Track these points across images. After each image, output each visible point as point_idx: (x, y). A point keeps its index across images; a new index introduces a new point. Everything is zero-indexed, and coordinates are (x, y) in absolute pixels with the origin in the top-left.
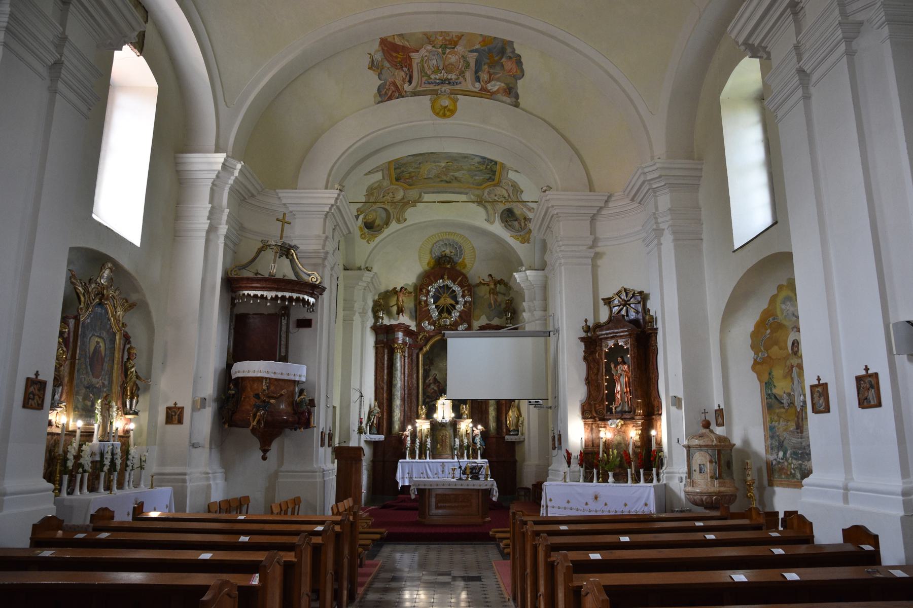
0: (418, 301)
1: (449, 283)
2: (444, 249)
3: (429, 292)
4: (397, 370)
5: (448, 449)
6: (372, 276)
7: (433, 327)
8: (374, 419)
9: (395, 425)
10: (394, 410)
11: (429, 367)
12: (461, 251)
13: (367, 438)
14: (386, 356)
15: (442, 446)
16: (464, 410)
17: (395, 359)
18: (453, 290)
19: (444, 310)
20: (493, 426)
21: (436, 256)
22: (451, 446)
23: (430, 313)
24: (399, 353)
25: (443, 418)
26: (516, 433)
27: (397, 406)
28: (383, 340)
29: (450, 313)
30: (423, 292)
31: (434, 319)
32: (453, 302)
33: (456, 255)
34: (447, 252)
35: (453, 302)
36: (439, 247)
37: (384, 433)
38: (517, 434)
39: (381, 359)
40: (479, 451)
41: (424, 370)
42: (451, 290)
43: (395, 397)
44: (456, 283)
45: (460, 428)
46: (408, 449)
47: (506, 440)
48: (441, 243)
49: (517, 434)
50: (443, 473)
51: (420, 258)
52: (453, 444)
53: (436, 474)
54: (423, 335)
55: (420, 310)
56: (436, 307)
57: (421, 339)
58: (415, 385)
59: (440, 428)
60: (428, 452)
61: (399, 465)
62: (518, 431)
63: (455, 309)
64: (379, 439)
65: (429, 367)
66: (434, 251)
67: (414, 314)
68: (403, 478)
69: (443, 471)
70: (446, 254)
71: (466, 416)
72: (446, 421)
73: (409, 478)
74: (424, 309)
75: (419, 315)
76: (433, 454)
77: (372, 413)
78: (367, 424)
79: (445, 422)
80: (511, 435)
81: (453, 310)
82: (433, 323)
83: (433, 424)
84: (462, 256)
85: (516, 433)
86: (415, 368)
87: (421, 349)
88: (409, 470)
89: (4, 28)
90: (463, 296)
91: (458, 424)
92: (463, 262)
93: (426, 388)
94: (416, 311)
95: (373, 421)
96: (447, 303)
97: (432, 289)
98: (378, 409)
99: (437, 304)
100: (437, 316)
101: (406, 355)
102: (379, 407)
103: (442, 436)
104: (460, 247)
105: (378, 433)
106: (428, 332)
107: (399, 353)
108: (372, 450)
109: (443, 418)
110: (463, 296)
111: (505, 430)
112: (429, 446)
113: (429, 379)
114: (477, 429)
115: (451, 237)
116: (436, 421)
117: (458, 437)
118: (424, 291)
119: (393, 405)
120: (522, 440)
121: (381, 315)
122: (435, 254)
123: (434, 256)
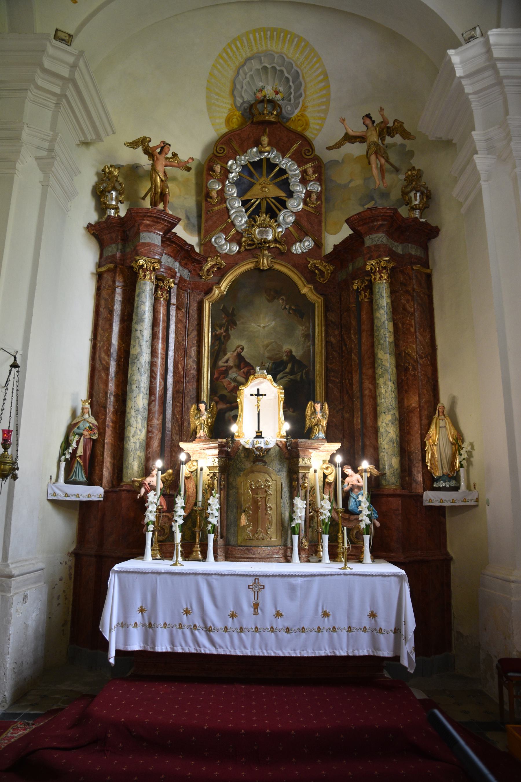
0: (204, 192)
1: (273, 155)
2: (261, 84)
3: (227, 172)
4: (142, 321)
5: (272, 530)
6: (71, 60)
7: (235, 248)
8: (78, 443)
9: (131, 459)
10: (128, 421)
11: (227, 331)
12: (298, 87)
13: (55, 494)
14: (119, 291)
15: (255, 520)
16: (319, 416)
17: (138, 295)
18: (281, 169)
19: (260, 209)
20: (391, 466)
21: (244, 102)
22: (282, 521)
23: (229, 217)
24: (148, 281)
25: (259, 435)
26: (453, 483)
27: (137, 411)
28: (114, 256)
29: (274, 216)
30: (214, 171)
31: (240, 230)
32: (281, 194)
33: (287, 98)
34: (269, 92)
35: (281, 194)
36: (251, 76)
37: (105, 481)
38: (456, 489)
39: (106, 300)
40: (367, 538)
41: (215, 338)
42: (277, 169)
43: (134, 387)
44: (288, 155)
45: (308, 468)
46: (151, 527)
47: (426, 503)
48: (255, 65)
49: (456, 489)
50: (256, 613)
51: (209, 107)
52: (287, 514)
53: (233, 615)
54: (213, 263)
55: (207, 212)
56: (244, 203)
57: (208, 270)
58: (194, 372)
59: (248, 465)
60: (211, 537)
61: (114, 582)
62: (457, 478)
63: (285, 208)
64: (89, 496)
65: (227, 331)
66: (238, 86)
67: (194, 221)
68: (124, 625)
69: (256, 606)
70: (265, 96)
71: (322, 435)
72: (267, 443)
73: (144, 625)
74: (216, 208)
75: (206, 221)
76: (227, 544)
77: (75, 430)
78: (60, 457)
79: (262, 445)
80: (439, 489)
81: (280, 210)
82: (237, 239)
83: (228, 453)
84: (301, 99)
85: (453, 483)
86: (195, 333)
87: (209, 291)
88: (144, 599)
89: (216, 455)
90: (304, 181)
91: (301, 454)
92: (302, 115)
93: (217, 379)
94: (199, 216)
95: (75, 450)
96: (268, 195)
97: (234, 167)
98: (92, 420)
99: (245, 198)
100: (246, 222)
101: (174, 301)
102: (95, 415)
103: (255, 491)
104: (297, 75)
105: (90, 482)
106: (226, 256)
107: (148, 281)
108: (75, 525)
109: (259, 435)
110: (304, 181)
111: (419, 478)
112: (214, 520)
113: (226, 357)
114: (356, 471)
115: (275, 47)
116: (237, 447)
117: (302, 493)
118: (218, 168)
119: (128, 410)
120: (473, 503)
121: (114, 203)
122: (242, 97)
123: (239, 101)
